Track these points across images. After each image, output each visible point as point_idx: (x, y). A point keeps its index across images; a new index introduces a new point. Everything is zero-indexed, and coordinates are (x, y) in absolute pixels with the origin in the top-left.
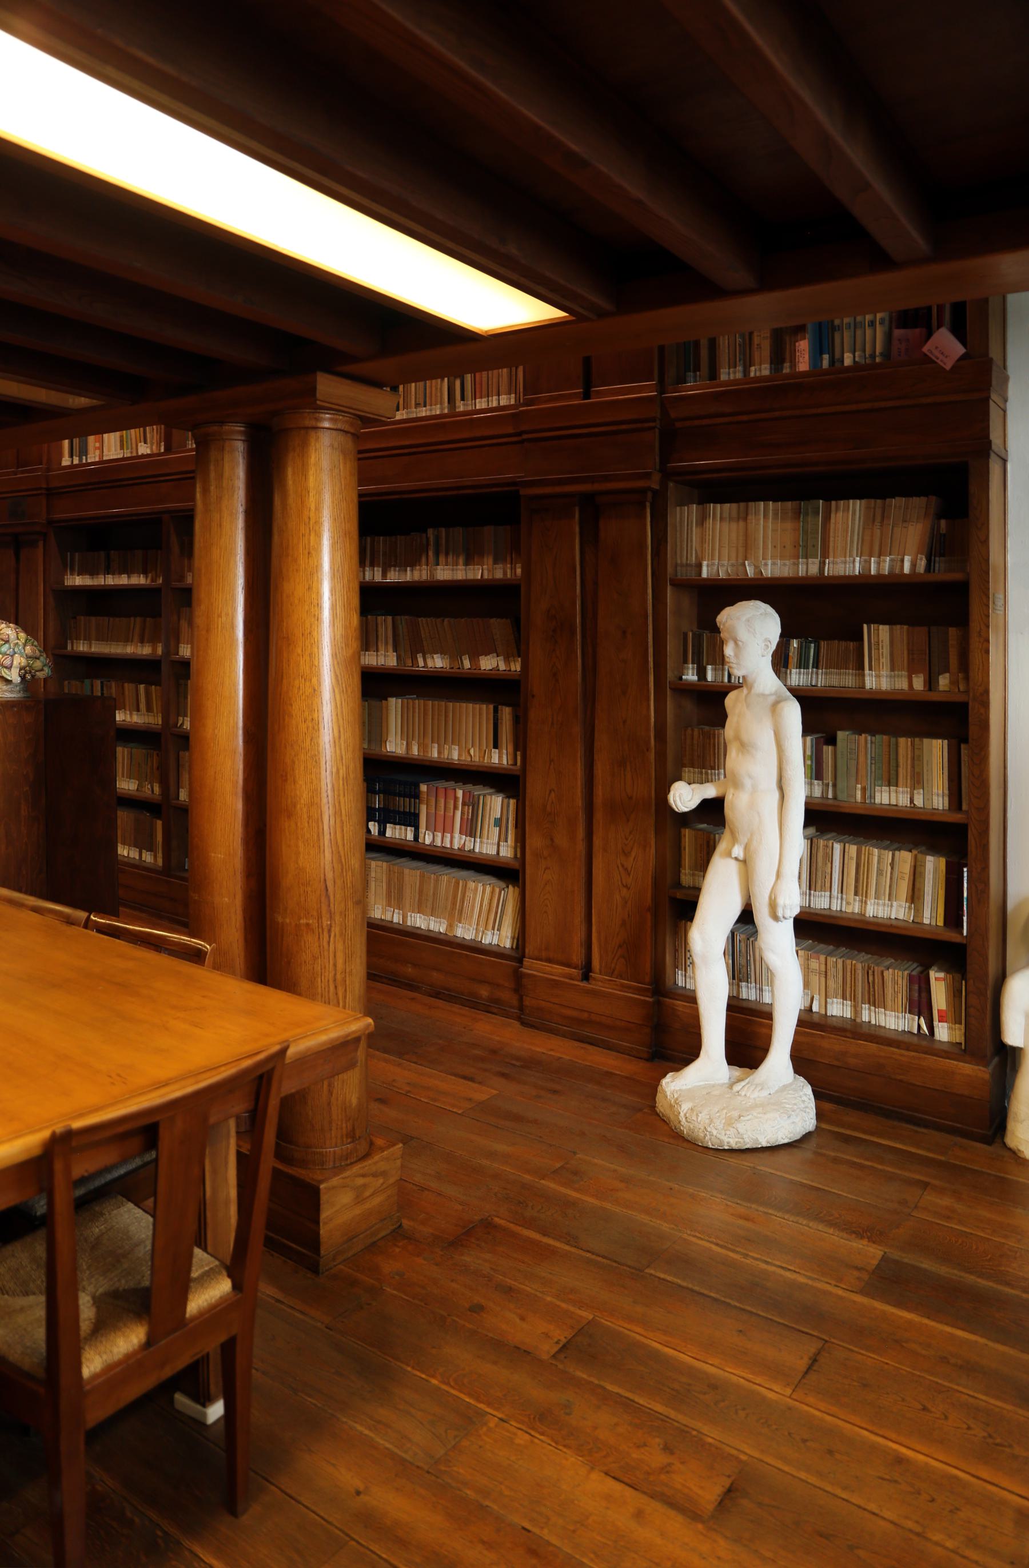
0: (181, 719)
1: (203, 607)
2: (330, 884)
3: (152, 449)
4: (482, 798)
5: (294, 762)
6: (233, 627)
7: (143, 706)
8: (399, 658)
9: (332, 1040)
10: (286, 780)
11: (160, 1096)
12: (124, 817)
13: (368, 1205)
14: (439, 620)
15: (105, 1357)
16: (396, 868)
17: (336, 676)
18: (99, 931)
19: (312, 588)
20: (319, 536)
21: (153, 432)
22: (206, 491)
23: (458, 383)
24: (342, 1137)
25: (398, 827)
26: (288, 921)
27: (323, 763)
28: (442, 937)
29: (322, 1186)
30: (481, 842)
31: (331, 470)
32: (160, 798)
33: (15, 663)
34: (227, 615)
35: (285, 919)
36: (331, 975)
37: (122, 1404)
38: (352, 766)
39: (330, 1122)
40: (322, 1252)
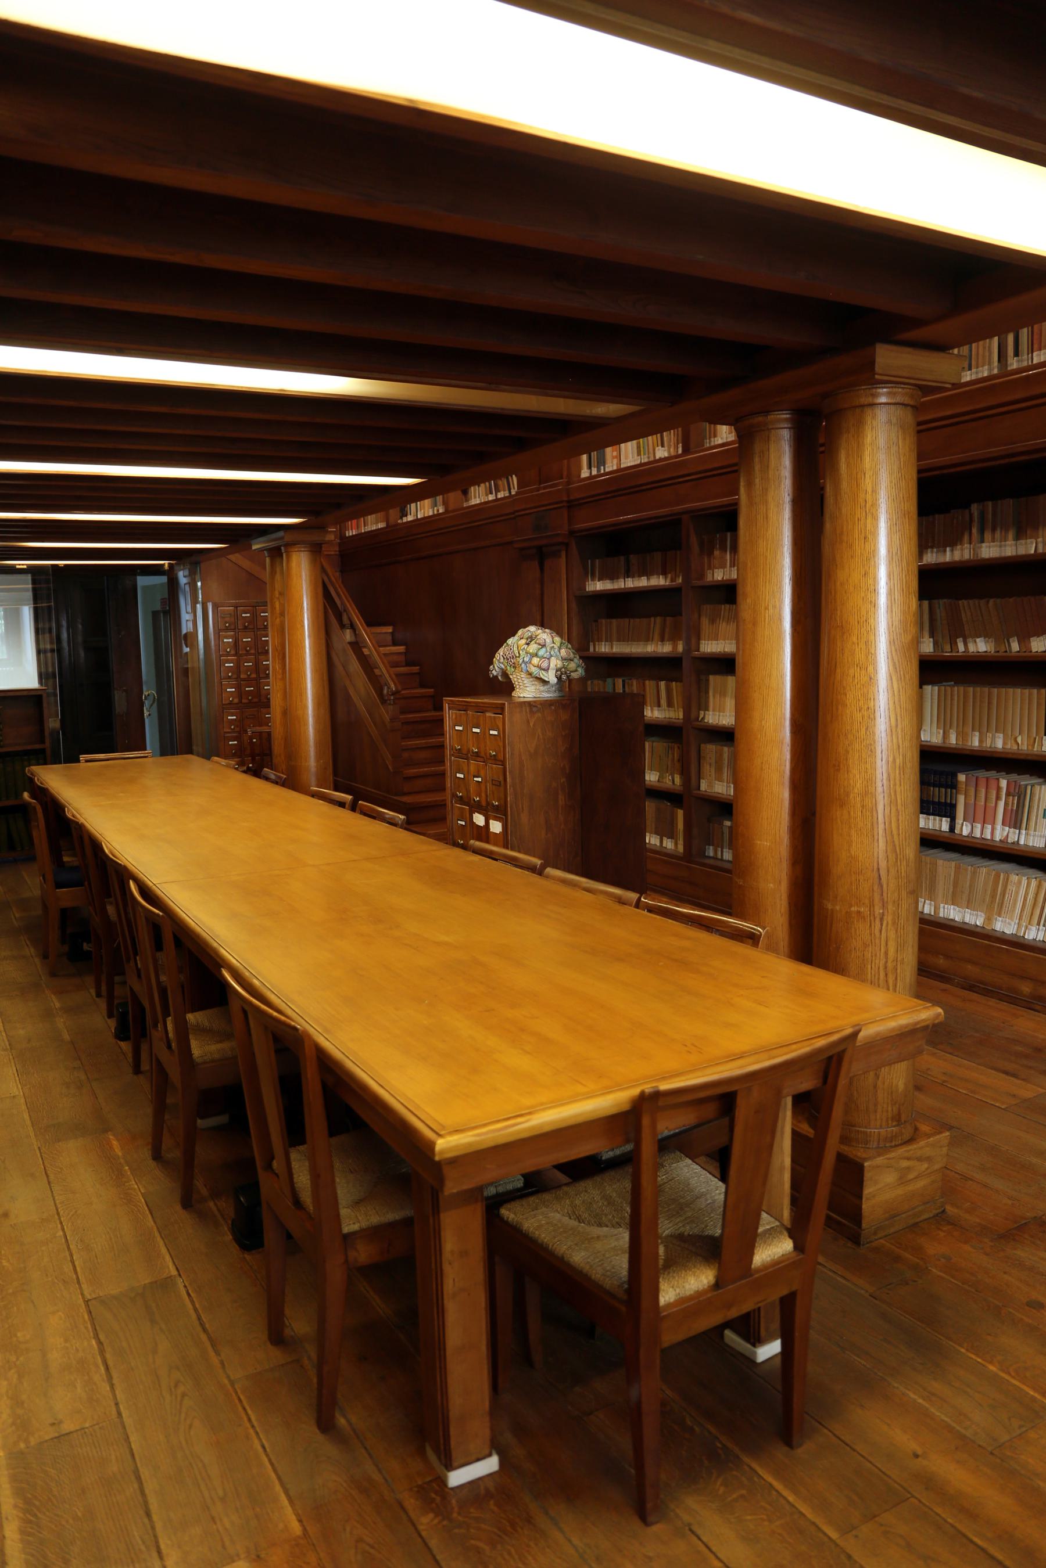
0: (702, 713)
1: (749, 601)
2: (883, 873)
3: (669, 451)
4: (1029, 788)
5: (847, 752)
6: (780, 619)
7: (664, 701)
8: (935, 644)
9: (901, 1027)
10: (838, 770)
11: (740, 1068)
12: (650, 807)
13: (911, 1187)
14: (983, 602)
15: (678, 1291)
16: (928, 859)
17: (894, 664)
18: (650, 911)
19: (869, 574)
20: (876, 519)
21: (670, 436)
22: (750, 484)
23: (1011, 338)
24: (887, 1120)
25: (932, 817)
26: (838, 908)
27: (879, 752)
28: (978, 930)
29: (866, 1164)
30: (1027, 834)
31: (889, 448)
32: (682, 788)
33: (552, 665)
34: (774, 607)
35: (834, 906)
36: (882, 962)
37: (693, 1333)
38: (909, 755)
39: (876, 1105)
40: (864, 1225)
